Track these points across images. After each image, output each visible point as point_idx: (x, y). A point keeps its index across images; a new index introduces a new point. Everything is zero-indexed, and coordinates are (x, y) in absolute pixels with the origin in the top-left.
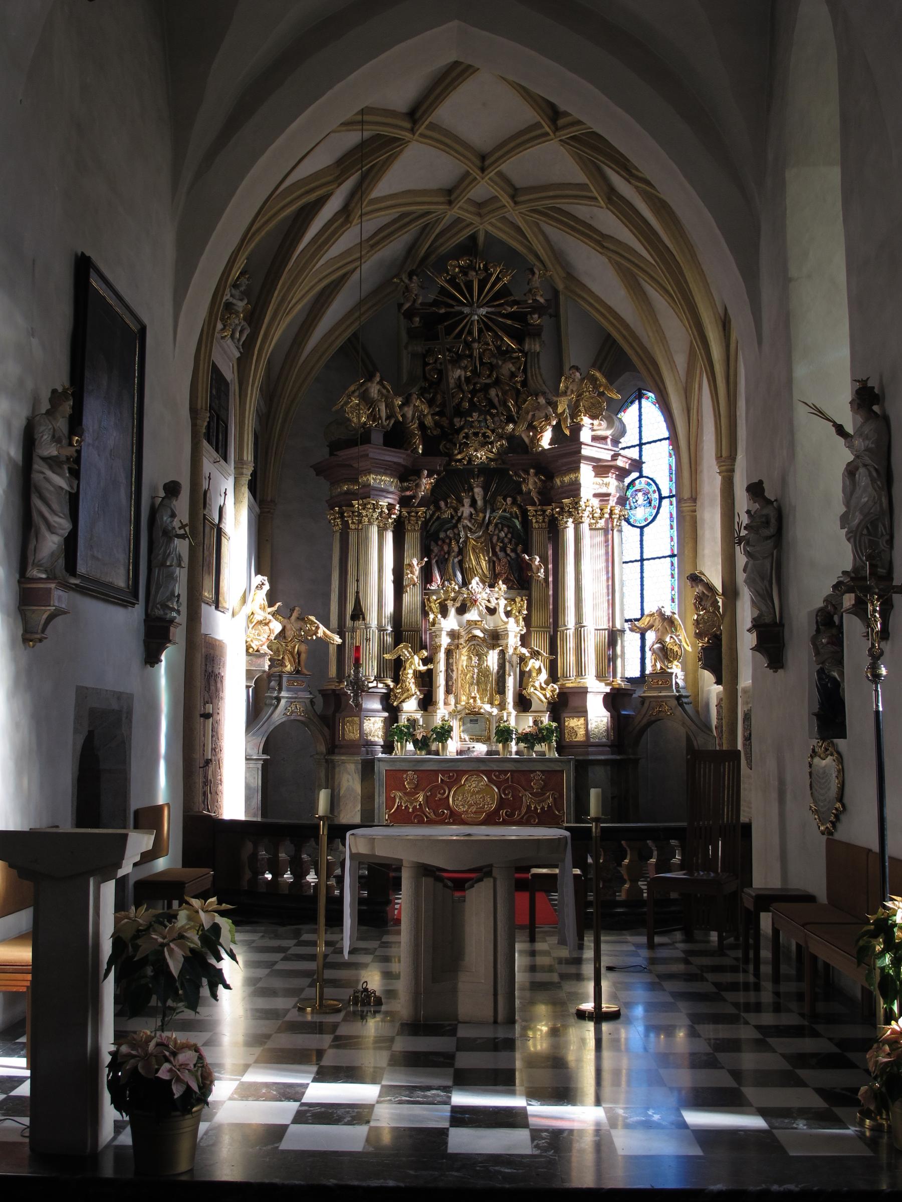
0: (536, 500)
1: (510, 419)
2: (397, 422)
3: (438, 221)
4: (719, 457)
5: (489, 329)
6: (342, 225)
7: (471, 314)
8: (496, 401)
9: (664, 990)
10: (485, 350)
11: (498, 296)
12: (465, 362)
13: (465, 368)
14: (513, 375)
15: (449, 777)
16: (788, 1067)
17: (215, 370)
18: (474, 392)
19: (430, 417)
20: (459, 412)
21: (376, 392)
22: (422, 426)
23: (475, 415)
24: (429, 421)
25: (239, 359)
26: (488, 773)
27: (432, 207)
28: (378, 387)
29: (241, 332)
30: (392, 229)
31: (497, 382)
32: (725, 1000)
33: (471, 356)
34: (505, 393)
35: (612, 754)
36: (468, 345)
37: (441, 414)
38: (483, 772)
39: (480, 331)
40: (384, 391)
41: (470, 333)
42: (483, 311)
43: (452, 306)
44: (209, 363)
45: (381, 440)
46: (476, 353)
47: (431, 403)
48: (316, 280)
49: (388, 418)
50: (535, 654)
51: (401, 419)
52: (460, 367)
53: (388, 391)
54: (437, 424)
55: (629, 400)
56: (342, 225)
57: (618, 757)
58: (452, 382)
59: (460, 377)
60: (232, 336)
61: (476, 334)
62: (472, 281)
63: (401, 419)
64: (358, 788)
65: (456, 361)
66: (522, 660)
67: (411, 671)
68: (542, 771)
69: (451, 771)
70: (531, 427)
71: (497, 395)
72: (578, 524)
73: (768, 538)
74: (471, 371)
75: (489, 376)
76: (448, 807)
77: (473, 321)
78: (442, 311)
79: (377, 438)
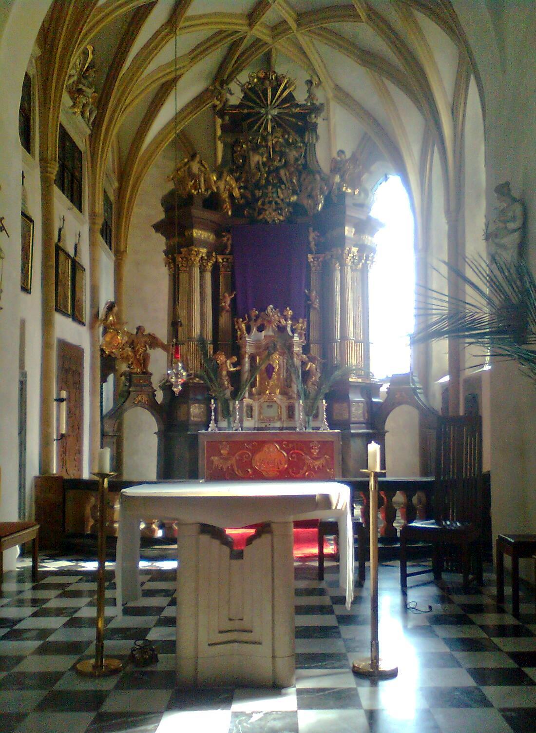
0: (313, 249)
1: (294, 192)
2: (213, 193)
3: (242, 39)
4: (448, 211)
5: (279, 125)
6: (167, 35)
7: (267, 114)
8: (284, 179)
9: (437, 636)
10: (276, 142)
11: (285, 100)
12: (262, 150)
13: (262, 155)
14: (297, 160)
15: (253, 446)
16: (462, 612)
17: (64, 135)
18: (269, 173)
19: (237, 190)
20: (257, 186)
21: (197, 169)
22: (231, 196)
23: (270, 188)
24: (236, 193)
25: (91, 136)
26: (280, 443)
27: (237, 28)
28: (199, 165)
29: (90, 113)
30: (208, 44)
31: (286, 165)
32: (472, 623)
33: (267, 146)
34: (291, 174)
35: (367, 429)
36: (265, 139)
37: (245, 188)
38: (277, 442)
39: (273, 128)
40: (203, 169)
41: (266, 129)
42: (275, 112)
43: (252, 108)
44: (57, 122)
45: (201, 204)
46: (270, 144)
47: (237, 180)
48: (152, 80)
49: (207, 190)
50: (312, 359)
51: (216, 190)
52: (258, 153)
53: (205, 168)
54: (242, 196)
55: (379, 183)
56: (167, 35)
57: (371, 431)
58: (253, 165)
59: (258, 162)
60: (82, 113)
61: (269, 129)
62: (266, 90)
63: (216, 190)
64: (187, 456)
65: (256, 148)
66: (304, 364)
67: (224, 373)
68: (319, 442)
69: (253, 441)
70: (310, 196)
71: (285, 175)
72: (343, 265)
73: (514, 231)
74: (267, 157)
75: (280, 160)
76: (252, 468)
77: (267, 120)
78: (246, 111)
79: (198, 202)
